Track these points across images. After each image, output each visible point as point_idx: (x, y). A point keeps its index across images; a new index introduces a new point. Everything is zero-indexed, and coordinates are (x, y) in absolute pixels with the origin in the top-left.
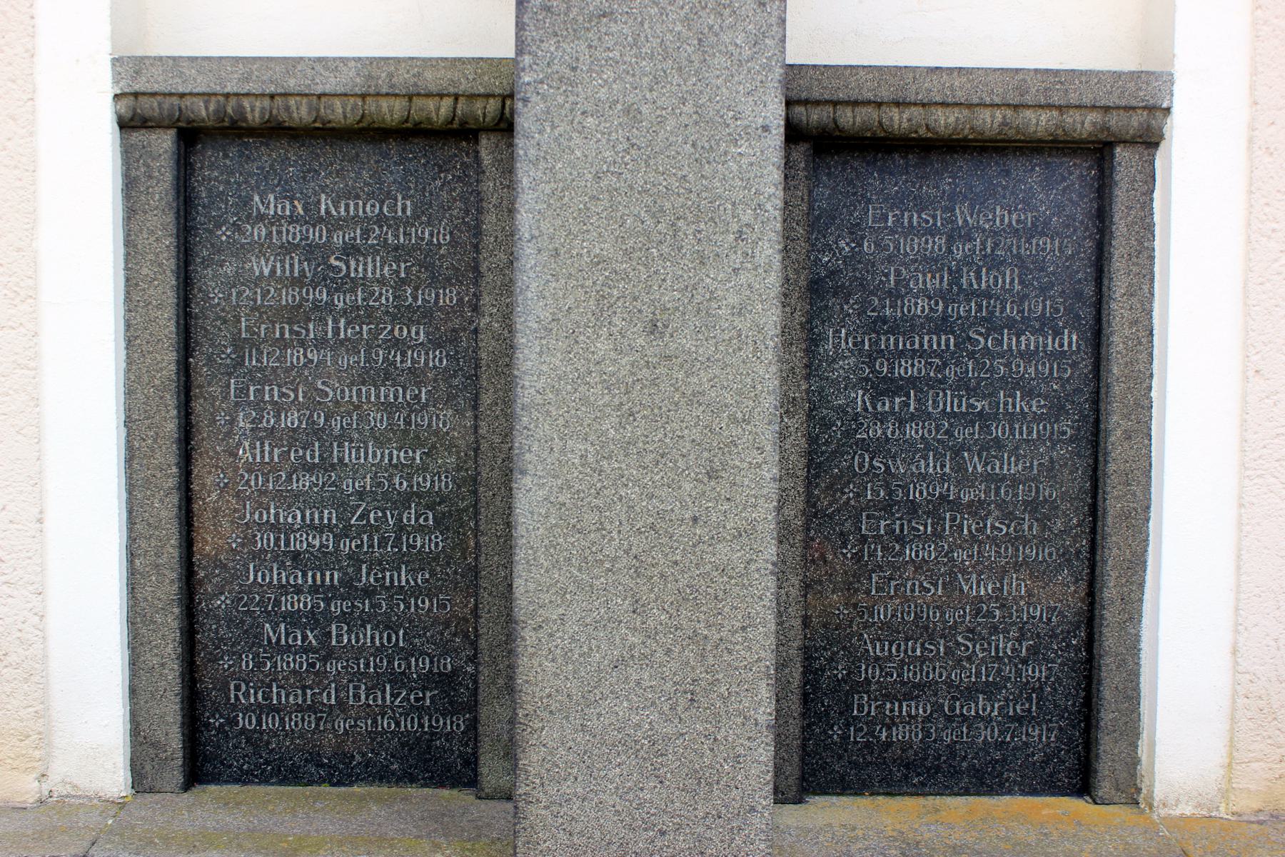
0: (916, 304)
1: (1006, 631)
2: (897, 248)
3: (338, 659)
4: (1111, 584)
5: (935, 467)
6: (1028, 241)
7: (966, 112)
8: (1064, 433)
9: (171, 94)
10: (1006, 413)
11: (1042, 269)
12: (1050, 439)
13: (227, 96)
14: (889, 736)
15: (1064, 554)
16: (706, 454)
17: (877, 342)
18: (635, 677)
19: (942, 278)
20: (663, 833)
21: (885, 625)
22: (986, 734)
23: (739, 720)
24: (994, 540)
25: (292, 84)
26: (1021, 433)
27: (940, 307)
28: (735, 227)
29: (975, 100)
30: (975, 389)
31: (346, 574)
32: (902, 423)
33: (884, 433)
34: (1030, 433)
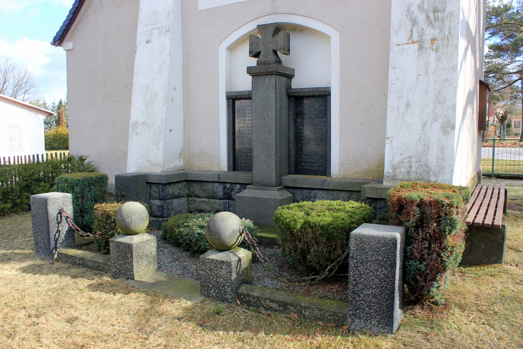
22: (316, 168)
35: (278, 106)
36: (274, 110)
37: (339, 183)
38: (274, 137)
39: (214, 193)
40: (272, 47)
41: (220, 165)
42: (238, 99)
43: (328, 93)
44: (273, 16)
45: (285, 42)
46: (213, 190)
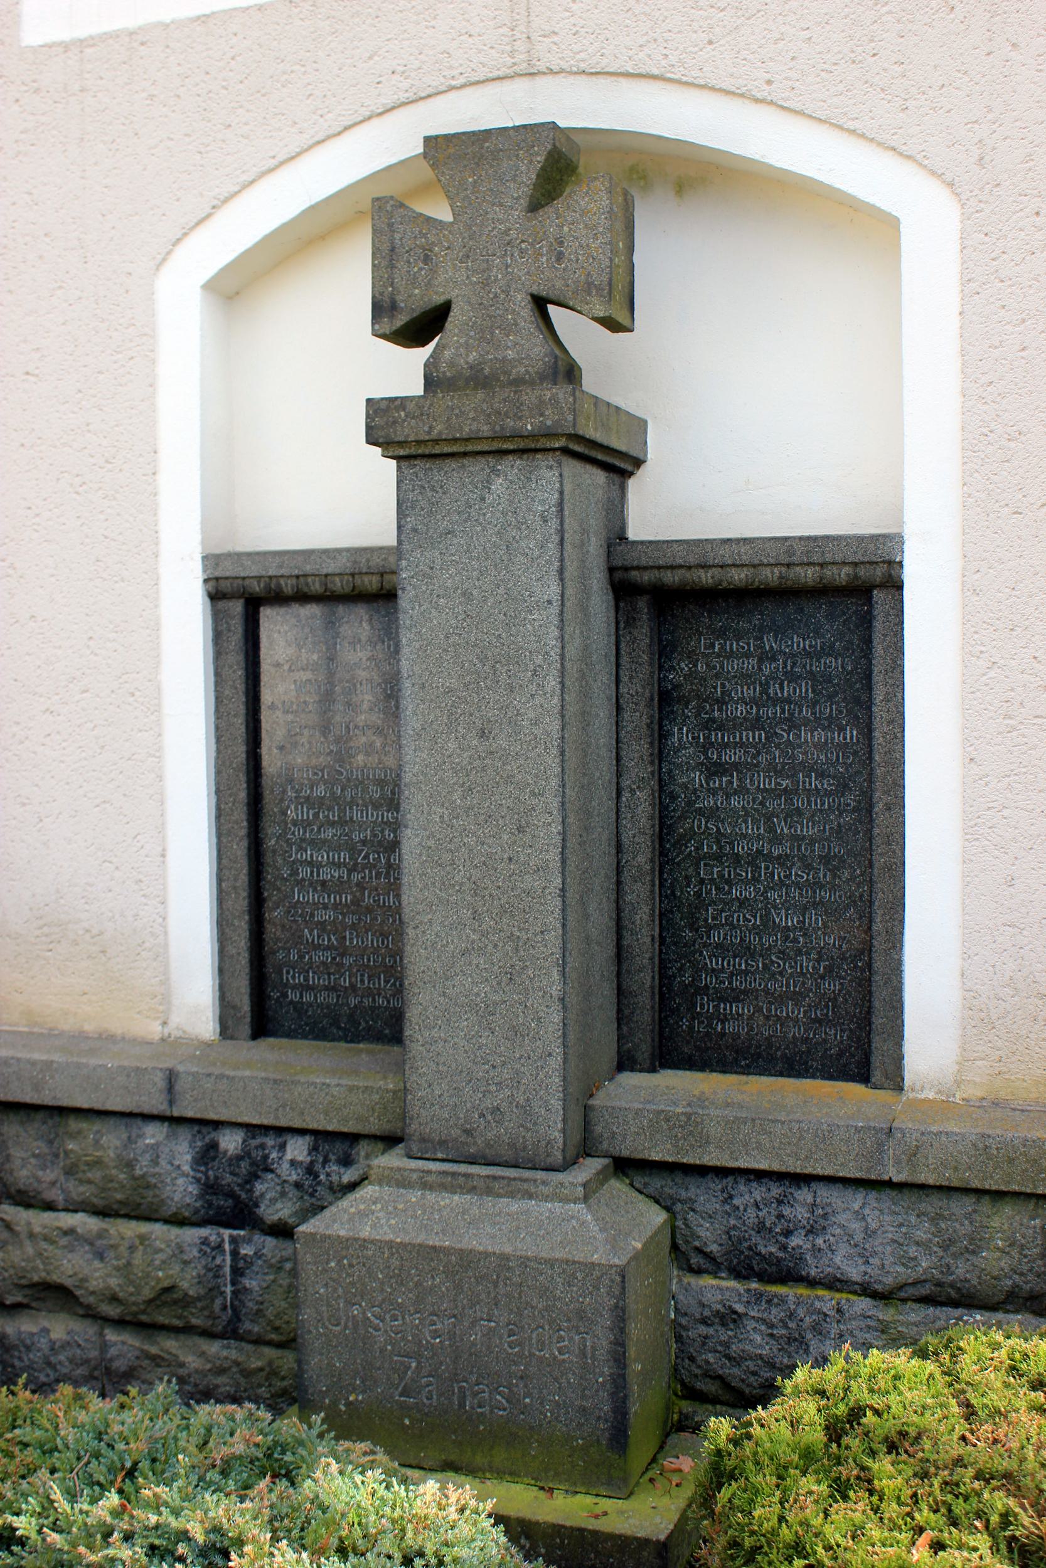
0: (737, 708)
1: (808, 954)
2: (722, 667)
3: (350, 955)
4: (878, 920)
5: (753, 829)
6: (818, 660)
7: (752, 570)
8: (848, 805)
9: (237, 578)
10: (805, 789)
11: (830, 681)
12: (838, 809)
13: (270, 577)
14: (723, 1028)
15: (850, 897)
16: (516, 816)
17: (709, 737)
18: (474, 962)
19: (755, 689)
20: (494, 1067)
21: (719, 946)
22: (793, 1032)
23: (540, 994)
24: (797, 884)
25: (308, 569)
26: (816, 805)
27: (754, 711)
28: (532, 667)
29: (756, 562)
30: (780, 772)
31: (355, 896)
32: (728, 796)
33: (716, 804)
34: (823, 804)
35: (572, 651)
36: (552, 683)
37: (983, 1148)
38: (553, 856)
39: (143, 1184)
40: (529, 274)
41: (166, 999)
42: (277, 597)
43: (880, 571)
44: (520, 86)
45: (614, 252)
46: (130, 1165)
